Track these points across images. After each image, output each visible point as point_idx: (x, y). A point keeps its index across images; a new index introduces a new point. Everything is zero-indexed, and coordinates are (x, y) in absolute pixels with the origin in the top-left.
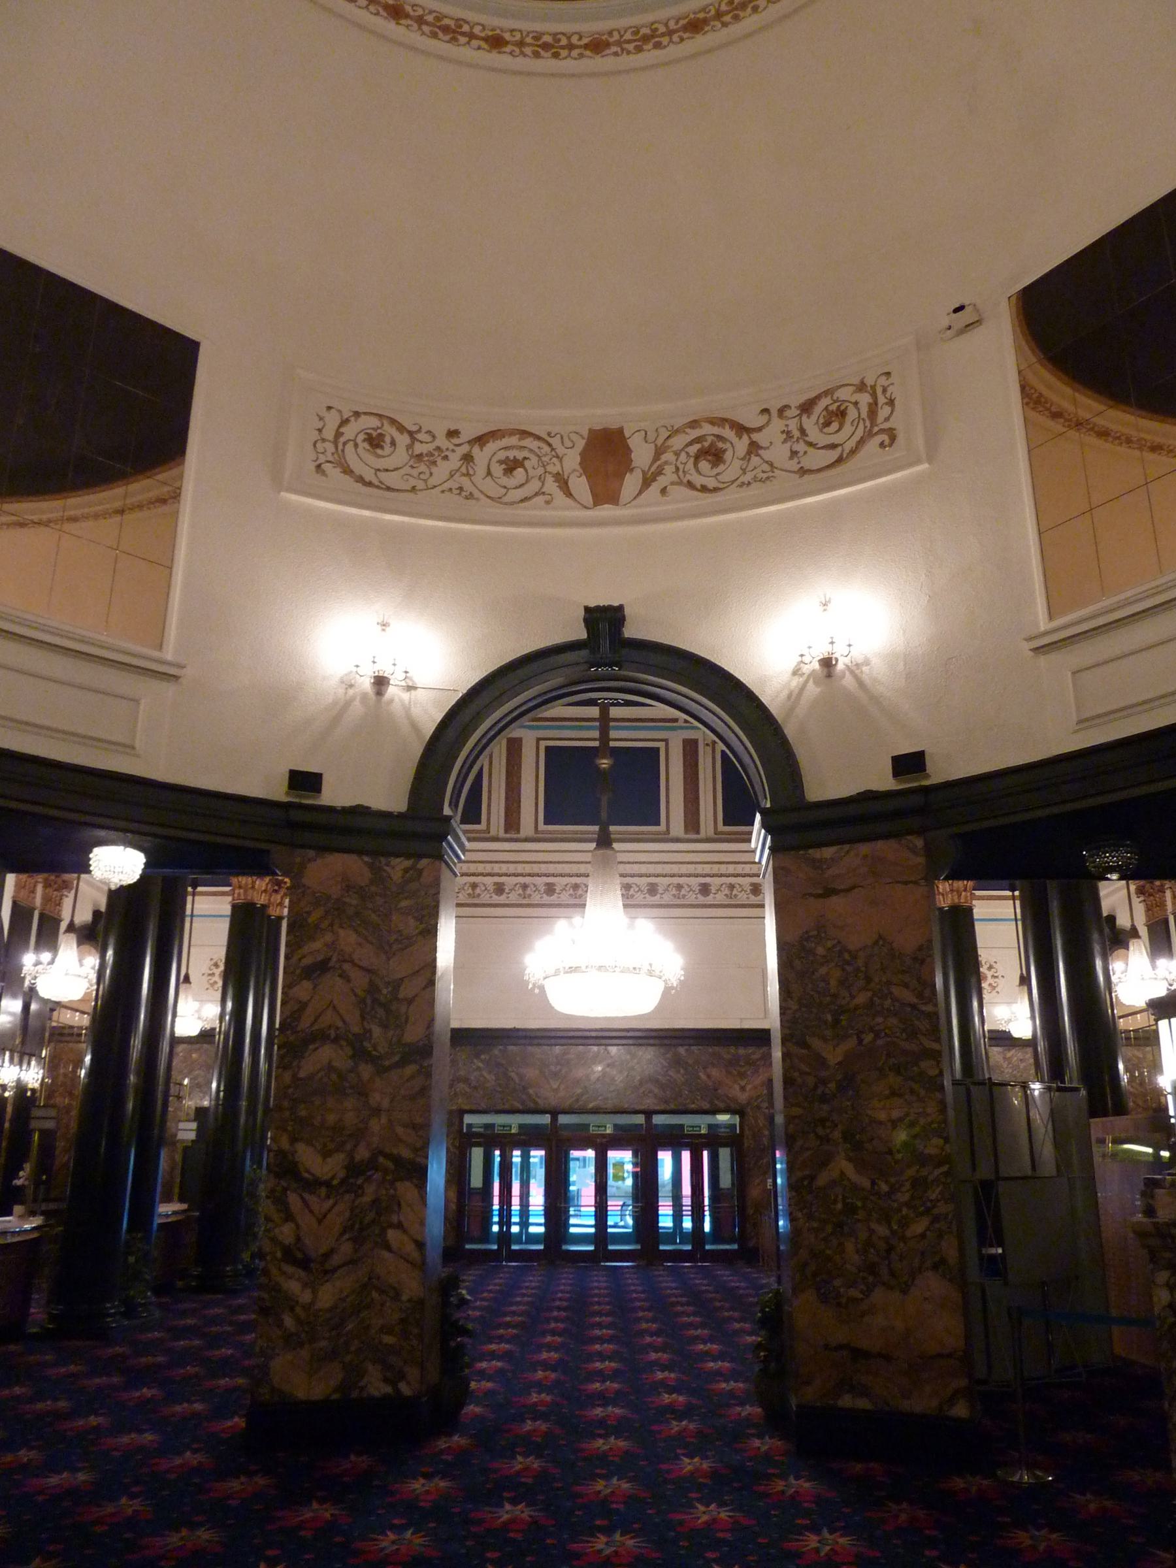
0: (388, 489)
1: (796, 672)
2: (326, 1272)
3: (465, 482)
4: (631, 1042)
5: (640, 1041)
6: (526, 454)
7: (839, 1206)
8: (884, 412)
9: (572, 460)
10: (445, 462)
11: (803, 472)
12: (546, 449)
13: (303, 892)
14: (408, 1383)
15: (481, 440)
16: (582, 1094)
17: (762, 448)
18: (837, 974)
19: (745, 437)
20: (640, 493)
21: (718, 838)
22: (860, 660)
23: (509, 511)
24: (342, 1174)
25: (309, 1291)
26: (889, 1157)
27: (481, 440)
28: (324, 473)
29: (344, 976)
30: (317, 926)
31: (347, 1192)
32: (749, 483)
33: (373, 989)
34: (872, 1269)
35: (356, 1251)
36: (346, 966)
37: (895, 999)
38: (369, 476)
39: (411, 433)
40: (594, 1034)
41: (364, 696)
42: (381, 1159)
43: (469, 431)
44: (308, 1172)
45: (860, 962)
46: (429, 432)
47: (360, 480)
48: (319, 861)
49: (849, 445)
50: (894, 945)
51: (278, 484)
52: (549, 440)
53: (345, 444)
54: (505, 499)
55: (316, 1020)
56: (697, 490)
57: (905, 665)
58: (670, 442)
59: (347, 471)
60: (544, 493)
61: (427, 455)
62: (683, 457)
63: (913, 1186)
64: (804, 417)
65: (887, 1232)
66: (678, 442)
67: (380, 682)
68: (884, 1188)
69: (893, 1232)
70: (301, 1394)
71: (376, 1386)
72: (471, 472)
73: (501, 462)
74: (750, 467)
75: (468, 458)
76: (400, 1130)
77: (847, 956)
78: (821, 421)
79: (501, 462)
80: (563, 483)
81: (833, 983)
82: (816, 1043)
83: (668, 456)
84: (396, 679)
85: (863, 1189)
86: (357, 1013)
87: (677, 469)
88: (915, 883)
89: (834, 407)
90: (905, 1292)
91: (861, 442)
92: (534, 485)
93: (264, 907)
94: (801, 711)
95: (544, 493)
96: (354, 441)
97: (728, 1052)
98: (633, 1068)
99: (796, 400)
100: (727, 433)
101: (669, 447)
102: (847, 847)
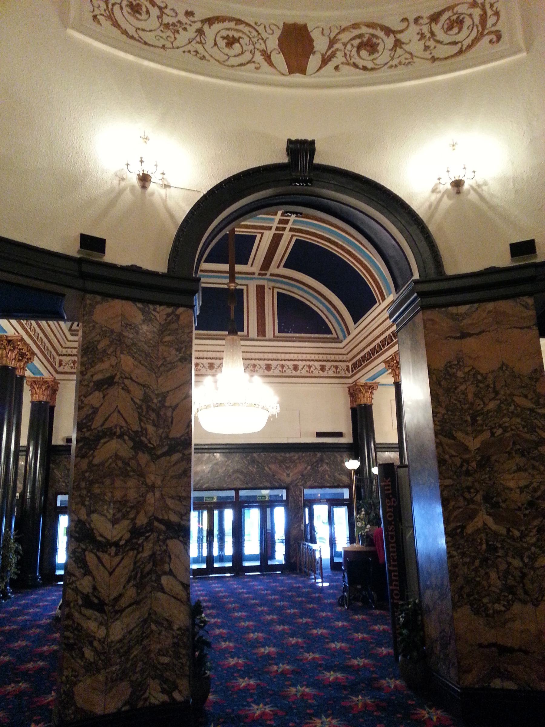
0: (146, 43)
1: (434, 191)
2: (116, 612)
3: (199, 47)
4: (227, 451)
5: (233, 451)
6: (240, 34)
7: (484, 547)
8: (491, 21)
9: (273, 43)
10: (185, 32)
11: (434, 59)
12: (254, 33)
13: (94, 326)
14: (180, 692)
15: (210, 21)
16: (200, 480)
17: (403, 43)
18: (472, 389)
19: (392, 36)
20: (320, 68)
21: (275, 339)
22: (480, 182)
23: (230, 71)
24: (127, 536)
25: (103, 628)
26: (519, 513)
27: (210, 21)
28: (99, 22)
29: (126, 389)
30: (105, 351)
31: (130, 550)
32: (396, 66)
33: (146, 399)
34: (511, 590)
35: (138, 594)
36: (127, 382)
37: (517, 406)
38: (132, 31)
39: (160, 8)
40: (207, 447)
41: (133, 188)
42: (156, 524)
43: (201, 14)
44: (101, 535)
45: (490, 381)
46: (173, 9)
47: (125, 32)
48: (104, 304)
49: (466, 43)
50: (515, 370)
51: (65, 24)
52: (256, 27)
53: (113, 5)
54: (227, 63)
55: (106, 420)
56: (360, 68)
57: (514, 185)
58: (339, 37)
59: (116, 24)
60: (254, 62)
61: (172, 25)
62: (349, 47)
63: (538, 531)
64: (433, 25)
65: (521, 565)
66: (345, 37)
67: (144, 179)
68: (517, 534)
69: (526, 565)
70: (99, 711)
71: (156, 696)
72: (203, 41)
73: (224, 38)
74: (396, 56)
75: (200, 32)
76: (169, 502)
77: (479, 377)
78: (446, 26)
79: (224, 38)
80: (268, 58)
81: (470, 396)
82: (460, 435)
83: (338, 46)
84: (155, 178)
85: (501, 535)
86: (136, 415)
87: (345, 54)
88: (529, 328)
89: (455, 17)
90: (536, 606)
91: (476, 41)
92: (247, 56)
93: (14, 369)
94: (438, 216)
95: (254, 62)
96: (120, 4)
97: (280, 456)
98: (228, 465)
99: (426, 14)
100: (381, 34)
101: (339, 40)
102: (476, 305)
